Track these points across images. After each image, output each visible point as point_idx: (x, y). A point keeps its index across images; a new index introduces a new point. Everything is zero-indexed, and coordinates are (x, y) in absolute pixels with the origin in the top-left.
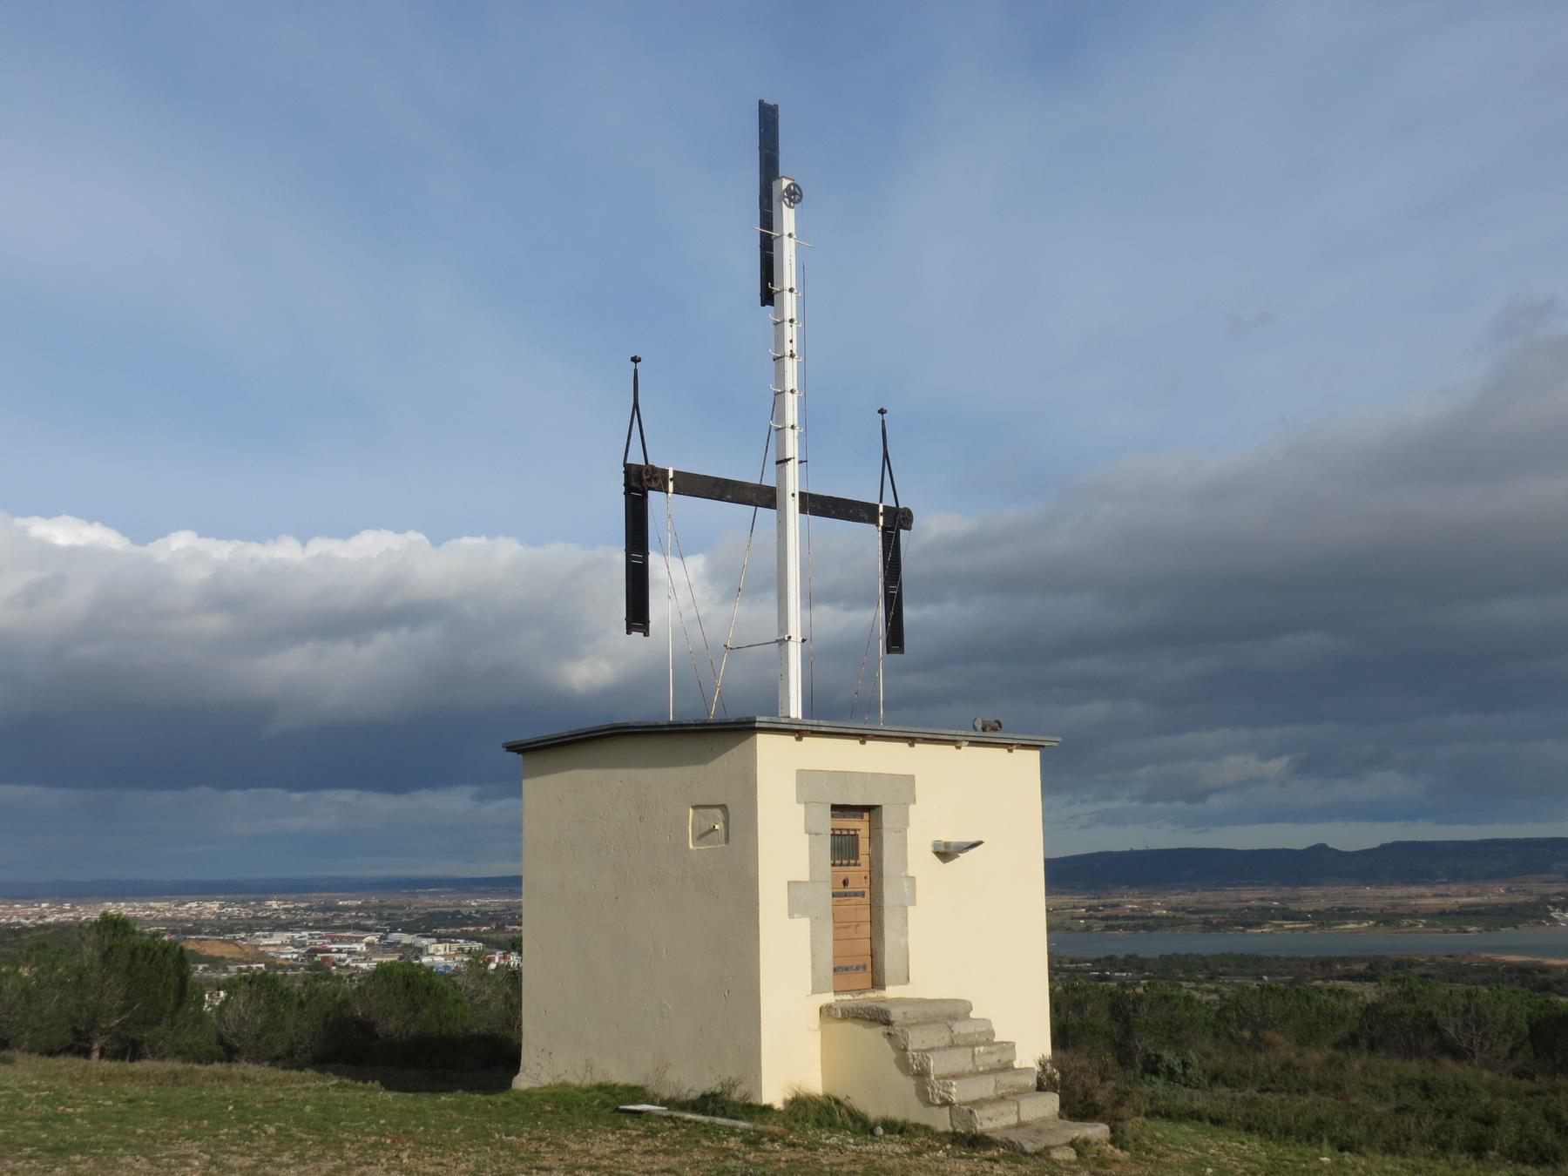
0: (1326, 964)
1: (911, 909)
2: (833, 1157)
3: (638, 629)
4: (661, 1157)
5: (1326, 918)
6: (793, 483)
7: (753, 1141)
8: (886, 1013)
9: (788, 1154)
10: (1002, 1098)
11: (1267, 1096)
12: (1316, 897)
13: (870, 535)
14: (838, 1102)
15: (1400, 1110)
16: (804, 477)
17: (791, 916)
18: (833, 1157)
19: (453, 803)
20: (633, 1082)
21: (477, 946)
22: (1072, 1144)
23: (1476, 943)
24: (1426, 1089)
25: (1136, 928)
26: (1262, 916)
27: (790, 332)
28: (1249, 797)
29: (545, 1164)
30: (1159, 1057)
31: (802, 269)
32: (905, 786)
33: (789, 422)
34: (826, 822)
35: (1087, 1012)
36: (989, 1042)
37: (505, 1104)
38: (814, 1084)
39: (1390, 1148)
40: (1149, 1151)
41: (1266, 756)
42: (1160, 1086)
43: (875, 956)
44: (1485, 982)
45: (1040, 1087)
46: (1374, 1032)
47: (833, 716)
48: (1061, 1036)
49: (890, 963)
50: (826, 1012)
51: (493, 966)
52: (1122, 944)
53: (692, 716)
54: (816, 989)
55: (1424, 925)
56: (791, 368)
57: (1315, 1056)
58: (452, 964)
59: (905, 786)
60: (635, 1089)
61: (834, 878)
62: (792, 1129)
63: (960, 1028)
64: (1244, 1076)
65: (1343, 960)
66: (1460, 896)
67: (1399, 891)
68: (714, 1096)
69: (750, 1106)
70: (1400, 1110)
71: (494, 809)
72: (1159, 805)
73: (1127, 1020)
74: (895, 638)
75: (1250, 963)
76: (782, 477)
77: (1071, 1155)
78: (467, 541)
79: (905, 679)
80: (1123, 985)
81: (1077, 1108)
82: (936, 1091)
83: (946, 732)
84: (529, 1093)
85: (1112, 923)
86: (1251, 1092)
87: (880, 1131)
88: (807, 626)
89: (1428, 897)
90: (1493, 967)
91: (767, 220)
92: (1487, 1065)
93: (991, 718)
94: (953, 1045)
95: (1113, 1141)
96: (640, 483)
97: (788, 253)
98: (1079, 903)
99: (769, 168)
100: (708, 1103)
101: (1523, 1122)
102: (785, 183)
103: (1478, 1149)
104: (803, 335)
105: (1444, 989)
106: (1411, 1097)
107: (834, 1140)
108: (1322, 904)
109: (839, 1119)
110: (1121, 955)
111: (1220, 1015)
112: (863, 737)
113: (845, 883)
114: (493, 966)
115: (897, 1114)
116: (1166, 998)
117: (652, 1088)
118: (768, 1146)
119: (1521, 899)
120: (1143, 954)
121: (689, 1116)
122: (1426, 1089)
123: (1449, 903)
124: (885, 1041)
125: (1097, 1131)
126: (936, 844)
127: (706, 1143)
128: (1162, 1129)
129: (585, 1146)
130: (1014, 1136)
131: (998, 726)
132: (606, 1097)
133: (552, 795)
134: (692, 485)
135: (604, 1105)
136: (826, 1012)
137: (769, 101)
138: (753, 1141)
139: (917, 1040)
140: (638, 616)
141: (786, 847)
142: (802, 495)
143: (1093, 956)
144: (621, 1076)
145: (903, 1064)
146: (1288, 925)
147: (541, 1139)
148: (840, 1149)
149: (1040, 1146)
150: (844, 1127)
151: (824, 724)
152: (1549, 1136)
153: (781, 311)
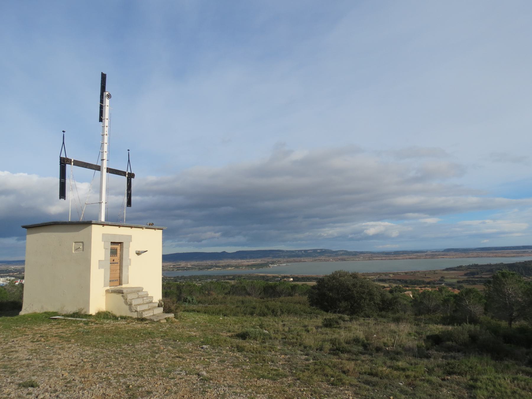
0: (224, 276)
2: (107, 326)
4: (61, 329)
5: (224, 267)
6: (105, 165)
7: (86, 323)
8: (122, 291)
9: (96, 326)
10: (150, 309)
11: (211, 306)
12: (223, 262)
13: (125, 179)
14: (109, 313)
15: (237, 307)
16: (108, 164)
18: (107, 326)
19: (11, 241)
21: (13, 278)
22: (165, 319)
23: (255, 272)
24: (243, 302)
25: (184, 270)
26: (211, 267)
27: (106, 129)
28: (212, 241)
29: (27, 334)
30: (187, 298)
31: (110, 114)
32: (129, 238)
34: (109, 246)
35: (171, 289)
36: (147, 297)
37: (17, 319)
38: (103, 308)
39: (235, 315)
40: (183, 319)
41: (215, 233)
42: (187, 304)
43: (120, 278)
44: (256, 280)
45: (159, 306)
46: (234, 290)
47: (113, 220)
49: (124, 279)
50: (107, 291)
51: (17, 283)
52: (180, 273)
53: (76, 219)
55: (244, 268)
56: (106, 138)
57: (220, 296)
58: (5, 283)
59: (129, 238)
60: (55, 313)
61: (111, 259)
62: (97, 320)
63: (140, 294)
64: (205, 301)
65: (228, 276)
66: (252, 262)
67: (240, 261)
68: (77, 313)
70: (237, 307)
71: (22, 242)
72: (191, 243)
73: (181, 290)
74: (129, 203)
75: (210, 277)
76: (102, 164)
77: (165, 321)
78: (21, 174)
79: (132, 212)
80: (181, 283)
82: (134, 308)
83: (140, 226)
84: (24, 316)
85: (178, 269)
86: (207, 305)
87: (119, 319)
88: (107, 199)
89: (245, 262)
90: (258, 276)
91: (102, 101)
93: (151, 223)
94: (138, 298)
96: (64, 162)
97: (107, 110)
98: (170, 264)
99: (103, 89)
100: (76, 315)
102: (107, 93)
103: (252, 314)
104: (110, 130)
105: (248, 281)
106: (239, 304)
107: (108, 322)
108: (224, 264)
110: (180, 276)
111: (201, 289)
112: (119, 226)
114: (17, 283)
115: (124, 314)
116: (189, 285)
117: (60, 312)
118: (90, 324)
119: (264, 262)
120: (185, 276)
121: (70, 318)
122: (243, 302)
123: (249, 263)
125: (171, 315)
126: (136, 251)
127: (74, 325)
128: (186, 314)
129: (39, 328)
130: (152, 318)
131: (153, 224)
132: (47, 315)
133: (34, 239)
134: (78, 163)
135: (46, 317)
136: (107, 291)
137: (104, 73)
138: (86, 323)
139: (129, 297)
140: (63, 194)
141: (99, 251)
143: (173, 276)
144: (51, 309)
145: (126, 303)
146: (217, 268)
147: (26, 327)
148: (109, 324)
149: (158, 320)
150: (110, 318)
151: (110, 223)
152: (266, 310)
153: (104, 124)
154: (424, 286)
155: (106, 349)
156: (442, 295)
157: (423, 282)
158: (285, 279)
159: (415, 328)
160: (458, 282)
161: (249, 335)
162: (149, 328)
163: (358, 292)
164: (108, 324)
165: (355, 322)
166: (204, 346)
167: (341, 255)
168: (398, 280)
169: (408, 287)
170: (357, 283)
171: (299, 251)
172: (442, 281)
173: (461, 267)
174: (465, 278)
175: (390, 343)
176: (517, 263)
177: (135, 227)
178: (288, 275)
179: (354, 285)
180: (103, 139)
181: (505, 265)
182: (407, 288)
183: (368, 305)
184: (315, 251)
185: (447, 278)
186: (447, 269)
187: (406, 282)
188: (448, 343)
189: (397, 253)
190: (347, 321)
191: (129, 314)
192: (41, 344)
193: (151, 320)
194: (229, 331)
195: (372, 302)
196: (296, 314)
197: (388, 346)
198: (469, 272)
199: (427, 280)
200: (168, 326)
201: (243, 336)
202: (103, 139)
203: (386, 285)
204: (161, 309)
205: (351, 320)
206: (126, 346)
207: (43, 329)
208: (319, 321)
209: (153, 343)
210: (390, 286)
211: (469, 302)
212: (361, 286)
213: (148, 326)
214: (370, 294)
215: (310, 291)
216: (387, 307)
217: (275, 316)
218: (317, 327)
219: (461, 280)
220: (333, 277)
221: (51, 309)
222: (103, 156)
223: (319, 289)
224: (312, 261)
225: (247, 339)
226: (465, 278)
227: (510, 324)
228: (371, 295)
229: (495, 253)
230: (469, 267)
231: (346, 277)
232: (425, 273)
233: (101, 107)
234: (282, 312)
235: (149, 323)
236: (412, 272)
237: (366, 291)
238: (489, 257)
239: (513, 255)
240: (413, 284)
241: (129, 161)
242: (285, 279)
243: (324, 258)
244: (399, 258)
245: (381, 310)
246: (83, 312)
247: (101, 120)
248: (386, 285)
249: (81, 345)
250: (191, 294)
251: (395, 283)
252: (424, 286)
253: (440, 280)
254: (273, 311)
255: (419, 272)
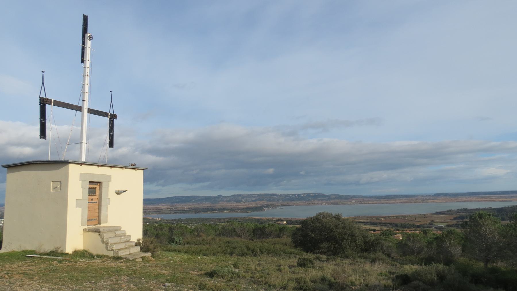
0: (220, 219)
1: (109, 206)
3: (43, 138)
6: (86, 106)
7: (60, 262)
8: (99, 230)
9: (69, 264)
13: (107, 120)
14: (86, 251)
16: (89, 105)
17: (76, 207)
20: (33, 249)
22: (142, 258)
25: (181, 213)
27: (88, 70)
31: (92, 56)
33: (86, 91)
34: (87, 186)
36: (125, 236)
38: (80, 247)
39: (214, 255)
43: (99, 217)
48: (145, 233)
50: (85, 230)
54: (82, 225)
56: (87, 79)
62: (72, 258)
63: (117, 233)
65: (224, 219)
69: (63, 253)
73: (172, 232)
76: (83, 104)
77: (141, 260)
81: (144, 249)
82: (110, 247)
87: (96, 257)
91: (84, 43)
92: (244, 238)
94: (115, 237)
95: (151, 256)
96: (44, 103)
97: (88, 52)
99: (85, 30)
100: (53, 253)
101: (241, 248)
102: (89, 35)
103: (231, 254)
109: (86, 255)
113: (92, 200)
115: (101, 253)
119: (258, 206)
121: (45, 257)
124: (99, 236)
125: (148, 254)
126: (116, 191)
127: (47, 263)
130: (127, 257)
134: (58, 104)
136: (85, 230)
137: (86, 14)
139: (106, 236)
142: (88, 109)
144: (29, 248)
145: (103, 242)
149: (133, 258)
150: (87, 257)
152: (246, 250)
153: (85, 65)
154: (414, 229)
155: (66, 286)
156: (427, 237)
157: (414, 226)
158: (279, 222)
159: (390, 268)
160: (448, 226)
161: (217, 273)
162: (122, 266)
163: (339, 233)
164: (82, 263)
165: (331, 262)
166: (167, 284)
167: (334, 199)
168: (389, 224)
169: (398, 230)
170: (339, 224)
171: (292, 195)
172: (432, 224)
173: (450, 211)
174: (455, 221)
175: (358, 283)
176: (505, 207)
177: (115, 167)
178: (282, 218)
179: (336, 226)
180: (84, 80)
181: (494, 209)
182: (398, 232)
183: (349, 246)
184: (308, 195)
185: (437, 222)
186: (437, 213)
187: (396, 225)
188: (415, 282)
189: (388, 198)
190: (324, 261)
191: (106, 253)
192: (3, 281)
193: (126, 258)
194: (201, 270)
195: (354, 243)
196: (276, 254)
197: (355, 286)
198: (458, 216)
199: (418, 224)
200: (143, 264)
201: (211, 275)
202: (84, 80)
203: (377, 228)
204: (138, 248)
205: (328, 260)
206: (88, 283)
207: (13, 267)
208: (294, 261)
209: (117, 280)
210: (381, 230)
211: (450, 244)
212: (344, 228)
213: (122, 264)
214: (352, 235)
215: (294, 234)
216: (368, 248)
217: (255, 256)
218: (290, 267)
219: (450, 224)
220: (317, 219)
221: (29, 247)
222: (84, 97)
223: (303, 231)
224: (306, 205)
225: (215, 277)
226: (455, 221)
227: (486, 265)
228: (353, 236)
229: (484, 197)
230: (458, 211)
231: (329, 218)
232: (415, 217)
233: (83, 49)
234: (262, 252)
235: (124, 261)
236: (403, 216)
237: (348, 232)
238: (478, 201)
239: (501, 199)
240: (403, 228)
241: (111, 102)
242: (279, 222)
243: (317, 202)
244: (390, 202)
245: (363, 250)
246: (59, 251)
247: (83, 61)
248: (377, 228)
249: (43, 282)
250: (182, 235)
251: (386, 226)
252: (414, 229)
253: (430, 224)
254: (253, 251)
255: (409, 216)
